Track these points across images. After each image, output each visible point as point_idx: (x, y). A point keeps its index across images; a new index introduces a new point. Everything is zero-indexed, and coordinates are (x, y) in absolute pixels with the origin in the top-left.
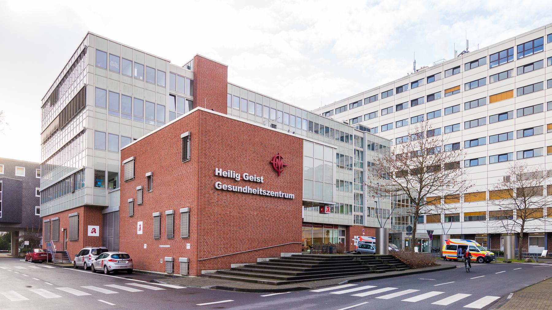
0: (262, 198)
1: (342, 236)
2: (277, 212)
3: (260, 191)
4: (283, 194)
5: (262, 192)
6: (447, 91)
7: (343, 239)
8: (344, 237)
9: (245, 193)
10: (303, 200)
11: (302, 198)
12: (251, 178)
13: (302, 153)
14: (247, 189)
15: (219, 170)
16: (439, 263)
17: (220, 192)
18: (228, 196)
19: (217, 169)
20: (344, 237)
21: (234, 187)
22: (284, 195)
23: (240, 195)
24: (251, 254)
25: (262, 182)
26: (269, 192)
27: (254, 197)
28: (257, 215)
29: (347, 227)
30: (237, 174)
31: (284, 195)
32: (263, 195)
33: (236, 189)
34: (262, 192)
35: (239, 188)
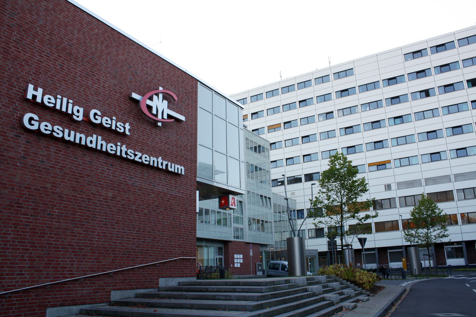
0: (125, 165)
1: (219, 255)
2: (153, 196)
3: (122, 149)
4: (165, 163)
5: (126, 153)
6: (270, 128)
7: (220, 259)
8: (222, 257)
9: (91, 149)
10: (198, 179)
11: (195, 176)
12: (106, 121)
13: (196, 102)
14: (95, 141)
15: (35, 89)
16: (335, 295)
17: (32, 138)
18: (53, 149)
19: (31, 87)
20: (222, 257)
21: (67, 131)
22: (167, 165)
23: (79, 152)
24: (270, 229)
25: (127, 133)
26: (139, 154)
27: (110, 161)
28: (114, 197)
29: (226, 243)
30: (76, 108)
31: (167, 165)
32: (127, 159)
33: (71, 136)
34: (126, 153)
35: (78, 135)
